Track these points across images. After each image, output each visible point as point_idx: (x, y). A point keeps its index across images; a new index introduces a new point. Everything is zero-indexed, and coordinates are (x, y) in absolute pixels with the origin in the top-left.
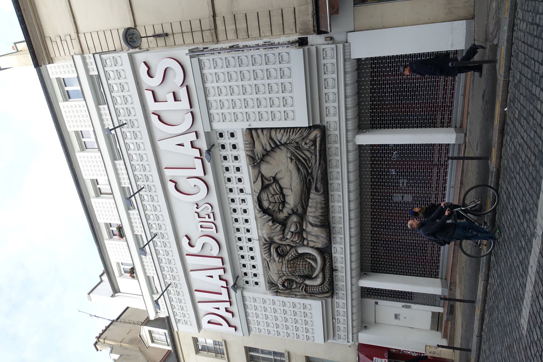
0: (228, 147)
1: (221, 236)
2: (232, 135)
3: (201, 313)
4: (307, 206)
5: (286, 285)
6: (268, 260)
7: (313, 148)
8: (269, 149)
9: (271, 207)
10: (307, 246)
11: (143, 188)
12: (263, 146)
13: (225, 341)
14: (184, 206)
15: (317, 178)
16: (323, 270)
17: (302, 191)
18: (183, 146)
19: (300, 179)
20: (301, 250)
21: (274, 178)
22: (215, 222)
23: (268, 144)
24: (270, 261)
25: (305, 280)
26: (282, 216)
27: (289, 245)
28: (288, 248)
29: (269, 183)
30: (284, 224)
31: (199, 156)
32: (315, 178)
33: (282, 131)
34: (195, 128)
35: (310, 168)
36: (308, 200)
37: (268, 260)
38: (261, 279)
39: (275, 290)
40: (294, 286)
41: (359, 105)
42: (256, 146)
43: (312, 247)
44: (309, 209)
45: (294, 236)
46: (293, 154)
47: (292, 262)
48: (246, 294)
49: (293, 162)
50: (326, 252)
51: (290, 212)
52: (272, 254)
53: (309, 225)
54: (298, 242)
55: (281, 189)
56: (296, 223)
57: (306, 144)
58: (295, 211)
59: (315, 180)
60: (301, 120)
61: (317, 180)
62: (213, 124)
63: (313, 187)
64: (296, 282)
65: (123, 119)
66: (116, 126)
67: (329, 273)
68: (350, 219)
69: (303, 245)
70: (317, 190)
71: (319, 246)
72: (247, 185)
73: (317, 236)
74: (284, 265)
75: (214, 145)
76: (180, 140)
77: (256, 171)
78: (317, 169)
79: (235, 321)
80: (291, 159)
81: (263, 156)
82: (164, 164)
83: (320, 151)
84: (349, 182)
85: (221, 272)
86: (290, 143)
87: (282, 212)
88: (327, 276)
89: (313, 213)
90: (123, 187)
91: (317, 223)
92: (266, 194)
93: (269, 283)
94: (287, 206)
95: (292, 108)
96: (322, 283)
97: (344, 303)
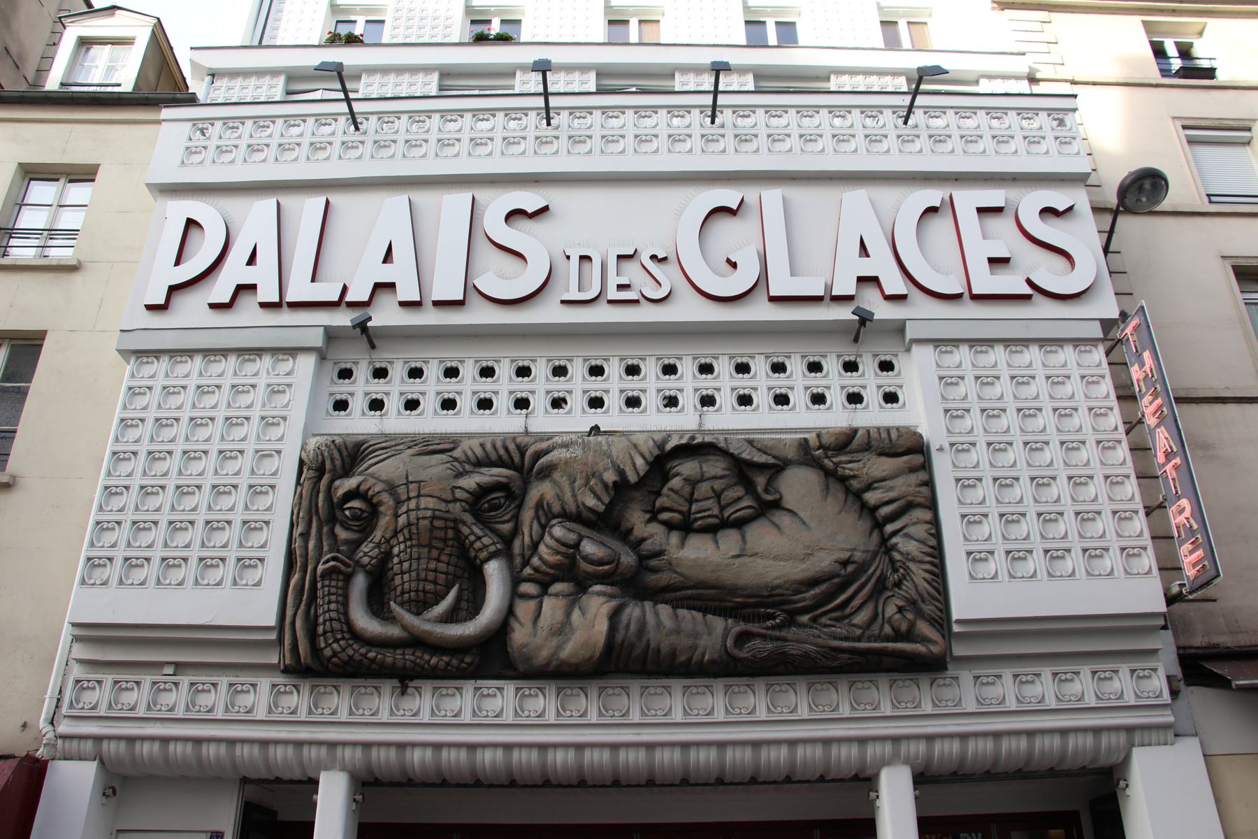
0: (378, 388)
1: (548, 313)
2: (891, 398)
3: (234, 205)
4: (676, 604)
5: (356, 504)
6: (456, 453)
7: (887, 629)
8: (872, 497)
9: (676, 483)
10: (514, 595)
11: (357, 129)
12: (882, 481)
13: (73, 269)
14: (671, 220)
15: (785, 640)
16: (417, 642)
17: (734, 590)
18: (385, 261)
19: (778, 587)
20: (494, 572)
21: (777, 505)
22: (603, 302)
23: (891, 495)
24: (456, 459)
25: (368, 573)
26: (636, 519)
27: (516, 531)
28: (506, 527)
29: (760, 489)
30: (605, 522)
31: (349, 298)
32: (783, 633)
33: (933, 542)
34: (475, 299)
35: (814, 619)
36: (699, 610)
37: (456, 453)
38: (358, 423)
39: (328, 465)
40: (342, 534)
41: (440, 783)
42: (884, 459)
43: (510, 612)
44: (665, 610)
45: (563, 549)
46: (862, 568)
47: (451, 533)
48: (307, 364)
49: (837, 566)
50: (491, 658)
51: (647, 547)
52: (484, 470)
53: (614, 603)
54: (535, 561)
55: (739, 524)
56: (614, 560)
57: (900, 610)
58: (653, 563)
59: (777, 633)
60: (969, 599)
61: (778, 639)
62: (928, 350)
63: (753, 627)
64: (356, 544)
65: (561, 119)
66: (551, 98)
67: (400, 664)
68: (615, 747)
69: (516, 580)
70: (743, 638)
71: (520, 635)
72: (764, 419)
73: (562, 629)
74: (443, 506)
75: (373, 346)
76: (404, 253)
77: (791, 453)
78: (819, 640)
79: (192, 310)
80: (845, 563)
81: (843, 480)
82: (337, 199)
83: (881, 653)
84: (756, 744)
85: (268, 293)
86: (892, 561)
87: (649, 521)
88: (389, 657)
89: (660, 621)
90: (514, 75)
91: (622, 631)
92: (720, 472)
93: (358, 445)
94: (675, 538)
95: (1081, 573)
96: (356, 636)
97: (262, 714)
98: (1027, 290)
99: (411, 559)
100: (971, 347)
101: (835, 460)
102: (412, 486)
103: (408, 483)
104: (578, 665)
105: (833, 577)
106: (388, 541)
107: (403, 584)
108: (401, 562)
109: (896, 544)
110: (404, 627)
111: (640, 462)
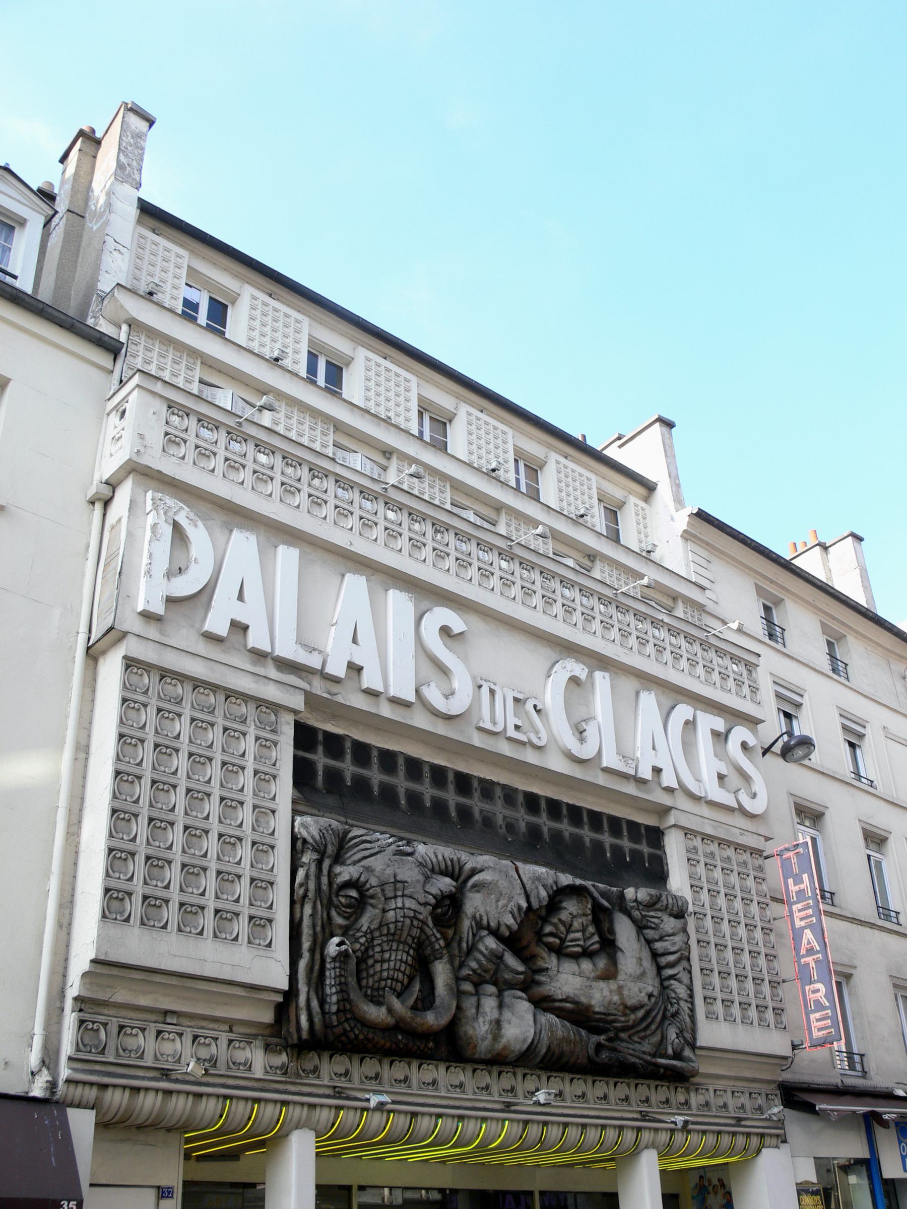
5: (354, 893)
8: (658, 946)
20: (442, 972)
99: (391, 949)
101: (643, 913)
102: (399, 885)
103: (396, 881)
106: (371, 932)
107: (382, 971)
108: (382, 951)
109: (671, 985)
110: (390, 1011)
111: (543, 893)
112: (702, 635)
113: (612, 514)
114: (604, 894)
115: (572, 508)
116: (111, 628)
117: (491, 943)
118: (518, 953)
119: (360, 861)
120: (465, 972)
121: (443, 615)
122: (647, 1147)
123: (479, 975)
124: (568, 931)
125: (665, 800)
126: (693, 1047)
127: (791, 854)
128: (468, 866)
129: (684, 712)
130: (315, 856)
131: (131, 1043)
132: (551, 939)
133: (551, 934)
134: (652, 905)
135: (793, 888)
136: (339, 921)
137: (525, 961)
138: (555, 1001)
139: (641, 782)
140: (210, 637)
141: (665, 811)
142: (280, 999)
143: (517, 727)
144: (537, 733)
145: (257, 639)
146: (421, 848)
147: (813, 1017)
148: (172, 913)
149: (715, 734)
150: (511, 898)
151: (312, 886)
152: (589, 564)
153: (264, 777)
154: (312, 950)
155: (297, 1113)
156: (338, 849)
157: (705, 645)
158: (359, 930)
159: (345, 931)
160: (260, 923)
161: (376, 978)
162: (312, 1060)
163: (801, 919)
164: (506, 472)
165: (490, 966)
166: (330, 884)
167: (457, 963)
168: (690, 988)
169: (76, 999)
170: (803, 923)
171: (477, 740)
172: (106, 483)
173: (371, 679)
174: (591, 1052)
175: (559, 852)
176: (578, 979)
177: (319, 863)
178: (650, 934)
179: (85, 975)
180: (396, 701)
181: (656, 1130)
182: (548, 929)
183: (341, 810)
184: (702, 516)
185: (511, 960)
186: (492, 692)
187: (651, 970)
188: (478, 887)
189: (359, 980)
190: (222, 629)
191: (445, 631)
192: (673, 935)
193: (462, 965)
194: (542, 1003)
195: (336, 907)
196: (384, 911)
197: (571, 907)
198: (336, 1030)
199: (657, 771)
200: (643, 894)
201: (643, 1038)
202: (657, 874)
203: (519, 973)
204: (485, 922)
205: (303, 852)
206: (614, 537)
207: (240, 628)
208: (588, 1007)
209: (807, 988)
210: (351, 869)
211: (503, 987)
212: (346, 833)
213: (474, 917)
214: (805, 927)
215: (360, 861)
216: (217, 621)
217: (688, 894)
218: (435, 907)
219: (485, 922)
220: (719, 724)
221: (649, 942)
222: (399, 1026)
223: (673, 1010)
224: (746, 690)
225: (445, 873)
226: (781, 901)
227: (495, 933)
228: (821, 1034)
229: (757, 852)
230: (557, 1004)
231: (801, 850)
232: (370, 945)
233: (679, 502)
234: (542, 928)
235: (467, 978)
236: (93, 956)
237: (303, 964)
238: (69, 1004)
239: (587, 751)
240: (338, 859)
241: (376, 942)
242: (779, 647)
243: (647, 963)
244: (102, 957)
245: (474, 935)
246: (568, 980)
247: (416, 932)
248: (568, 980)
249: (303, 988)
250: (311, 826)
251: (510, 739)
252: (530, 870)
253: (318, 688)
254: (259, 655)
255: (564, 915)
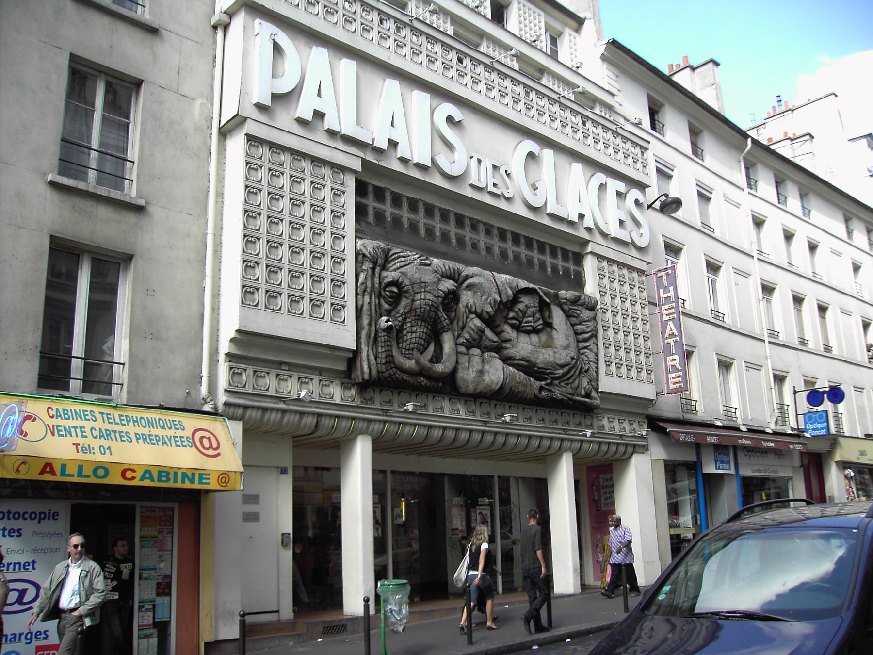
5: (395, 289)
50: (447, 386)
98: (429, 164)
100: (270, 148)
104: (485, 393)
105: (567, 365)
111: (510, 292)
112: (613, 127)
113: (554, 41)
114: (546, 294)
115: (528, 35)
116: (237, 115)
117: (478, 322)
118: (493, 329)
119: (398, 268)
120: (461, 340)
121: (449, 109)
122: (566, 451)
123: (470, 342)
124: (524, 317)
125: (585, 235)
126: (597, 390)
127: (663, 273)
128: (464, 274)
129: (601, 177)
130: (371, 265)
131: (261, 382)
132: (514, 322)
133: (513, 318)
134: (576, 301)
135: (663, 296)
136: (386, 306)
137: (498, 334)
138: (515, 360)
139: (571, 223)
140: (301, 122)
141: (585, 243)
142: (351, 356)
143: (495, 185)
144: (508, 188)
145: (330, 122)
146: (436, 261)
147: (670, 376)
148: (283, 301)
149: (619, 194)
150: (490, 295)
151: (369, 284)
152: (540, 75)
153: (337, 215)
154: (370, 324)
155: (361, 425)
156: (382, 261)
157: (615, 134)
158: (398, 313)
159: (389, 313)
160: (337, 309)
161: (408, 342)
162: (370, 393)
163: (667, 315)
164: (485, 8)
165: (476, 337)
166: (380, 283)
167: (456, 334)
168: (597, 354)
169: (226, 354)
170: (668, 318)
171: (469, 193)
172: (225, 12)
173: (402, 151)
174: (537, 391)
175: (520, 268)
176: (530, 347)
177: (373, 269)
178: (574, 320)
179: (232, 340)
180: (420, 166)
181: (572, 440)
182: (511, 315)
183: (385, 239)
184: (614, 43)
185: (488, 333)
186: (479, 161)
187: (573, 344)
188: (470, 287)
189: (398, 344)
190: (309, 116)
191: (450, 120)
192: (588, 321)
193: (459, 336)
194: (507, 360)
195: (384, 298)
196: (413, 301)
197: (525, 300)
198: (384, 374)
199: (581, 216)
200: (570, 294)
201: (567, 384)
202: (579, 282)
203: (494, 342)
204: (473, 309)
205: (362, 263)
206: (554, 56)
207: (319, 115)
208: (535, 365)
209: (668, 358)
210: (393, 273)
211: (485, 349)
212: (389, 250)
213: (467, 306)
214: (669, 320)
215: (398, 268)
216: (305, 110)
217: (598, 297)
218: (444, 299)
219: (473, 309)
220: (621, 186)
221: (573, 325)
222: (422, 372)
223: (586, 368)
224: (639, 165)
225: (450, 277)
226: (655, 305)
227: (479, 316)
228: (674, 386)
229: (641, 272)
230: (516, 362)
231: (669, 271)
232: (404, 322)
233: (599, 33)
234: (508, 314)
235: (462, 344)
236: (237, 328)
237: (364, 333)
238: (222, 357)
239: (537, 203)
240: (384, 268)
241: (408, 320)
242: (660, 137)
243: (572, 339)
244: (243, 329)
245: (467, 318)
246: (523, 346)
247: (432, 314)
248: (523, 346)
249: (364, 348)
250: (369, 245)
251: (491, 193)
252: (503, 278)
253: (370, 157)
254: (332, 133)
255: (521, 306)
